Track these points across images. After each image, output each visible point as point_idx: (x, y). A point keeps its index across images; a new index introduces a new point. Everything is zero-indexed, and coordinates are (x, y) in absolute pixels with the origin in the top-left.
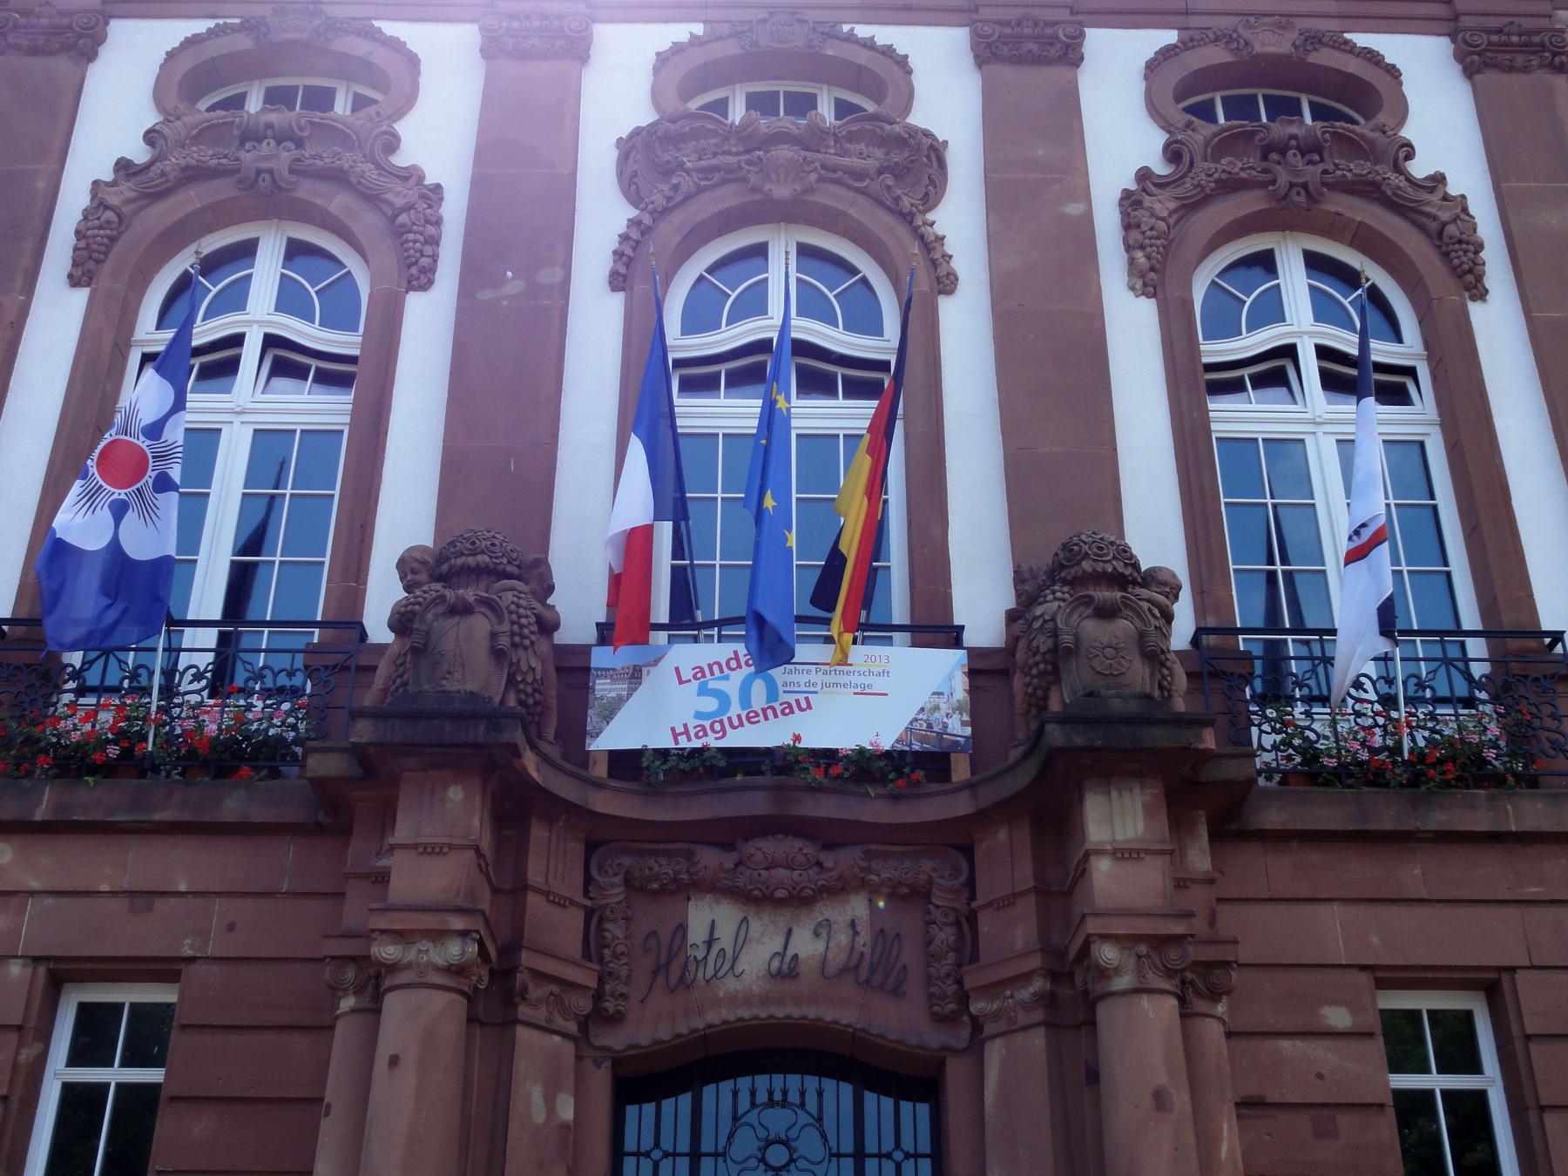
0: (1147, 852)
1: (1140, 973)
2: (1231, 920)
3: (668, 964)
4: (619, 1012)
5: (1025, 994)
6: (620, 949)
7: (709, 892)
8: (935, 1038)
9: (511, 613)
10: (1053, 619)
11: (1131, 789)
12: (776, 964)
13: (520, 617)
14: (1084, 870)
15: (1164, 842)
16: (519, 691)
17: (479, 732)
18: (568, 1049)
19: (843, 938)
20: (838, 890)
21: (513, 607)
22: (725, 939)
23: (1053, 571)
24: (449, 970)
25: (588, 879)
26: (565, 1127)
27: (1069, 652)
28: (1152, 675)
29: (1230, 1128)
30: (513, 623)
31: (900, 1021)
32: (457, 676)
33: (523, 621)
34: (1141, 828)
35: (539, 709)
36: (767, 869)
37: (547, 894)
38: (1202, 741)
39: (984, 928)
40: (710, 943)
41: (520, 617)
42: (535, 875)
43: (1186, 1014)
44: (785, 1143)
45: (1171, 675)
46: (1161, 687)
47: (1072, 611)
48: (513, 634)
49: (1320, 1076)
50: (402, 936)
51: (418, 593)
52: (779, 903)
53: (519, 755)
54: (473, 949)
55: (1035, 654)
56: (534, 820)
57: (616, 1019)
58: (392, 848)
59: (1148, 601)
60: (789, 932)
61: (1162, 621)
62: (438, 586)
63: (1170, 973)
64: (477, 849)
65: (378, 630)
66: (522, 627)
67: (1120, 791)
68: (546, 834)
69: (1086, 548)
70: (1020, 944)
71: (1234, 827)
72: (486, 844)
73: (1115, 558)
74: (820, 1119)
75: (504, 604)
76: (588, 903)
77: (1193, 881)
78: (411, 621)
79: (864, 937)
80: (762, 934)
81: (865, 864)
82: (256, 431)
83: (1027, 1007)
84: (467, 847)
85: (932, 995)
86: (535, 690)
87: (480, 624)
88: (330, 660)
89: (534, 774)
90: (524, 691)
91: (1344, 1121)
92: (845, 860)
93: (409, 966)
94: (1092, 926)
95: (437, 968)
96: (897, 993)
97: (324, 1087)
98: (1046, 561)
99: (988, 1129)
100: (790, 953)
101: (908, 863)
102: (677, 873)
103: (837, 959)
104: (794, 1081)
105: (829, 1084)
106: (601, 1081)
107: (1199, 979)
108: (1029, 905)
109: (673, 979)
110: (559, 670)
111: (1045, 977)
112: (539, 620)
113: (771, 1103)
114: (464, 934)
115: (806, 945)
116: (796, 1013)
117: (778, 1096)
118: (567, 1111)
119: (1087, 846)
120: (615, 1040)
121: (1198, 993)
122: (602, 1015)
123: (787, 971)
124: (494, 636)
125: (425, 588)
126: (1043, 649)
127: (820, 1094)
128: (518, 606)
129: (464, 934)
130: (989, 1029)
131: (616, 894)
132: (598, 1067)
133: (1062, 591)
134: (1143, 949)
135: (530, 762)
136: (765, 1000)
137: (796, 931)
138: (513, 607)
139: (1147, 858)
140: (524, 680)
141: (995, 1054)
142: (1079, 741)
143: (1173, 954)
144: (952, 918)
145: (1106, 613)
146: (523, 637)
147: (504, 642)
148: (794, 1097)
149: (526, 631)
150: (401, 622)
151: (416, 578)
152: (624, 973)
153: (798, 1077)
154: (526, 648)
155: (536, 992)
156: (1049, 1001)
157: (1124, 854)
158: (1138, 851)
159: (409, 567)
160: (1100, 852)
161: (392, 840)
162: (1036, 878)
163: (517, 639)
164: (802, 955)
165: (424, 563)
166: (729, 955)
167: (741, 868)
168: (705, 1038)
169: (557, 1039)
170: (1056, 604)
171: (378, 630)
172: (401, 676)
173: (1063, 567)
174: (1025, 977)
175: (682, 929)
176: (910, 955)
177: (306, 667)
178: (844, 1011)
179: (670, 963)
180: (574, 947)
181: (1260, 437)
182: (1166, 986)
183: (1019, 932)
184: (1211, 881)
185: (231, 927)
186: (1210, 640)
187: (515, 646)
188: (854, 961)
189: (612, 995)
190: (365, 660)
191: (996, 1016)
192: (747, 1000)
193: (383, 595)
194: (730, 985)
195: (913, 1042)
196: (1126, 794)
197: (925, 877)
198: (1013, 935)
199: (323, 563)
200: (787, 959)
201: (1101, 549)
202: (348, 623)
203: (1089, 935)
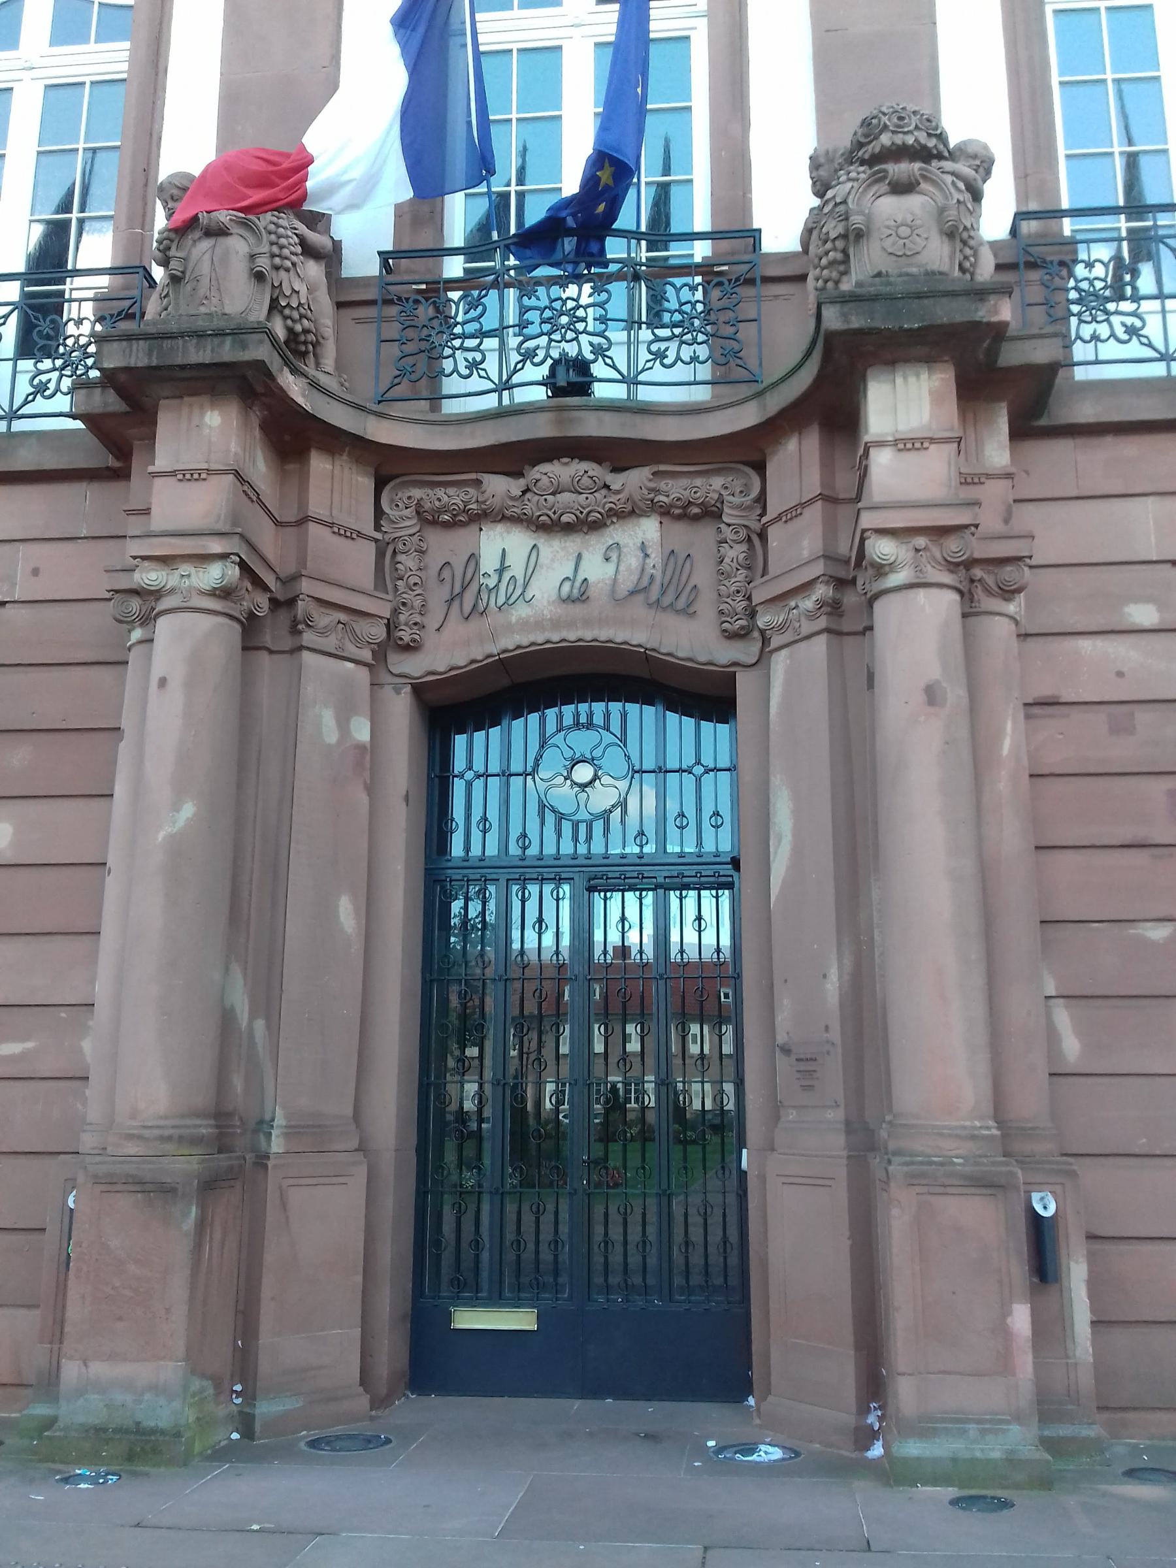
0: (932, 440)
1: (918, 568)
2: (1029, 517)
3: (461, 594)
4: (414, 641)
5: (808, 604)
6: (412, 580)
7: (500, 521)
8: (724, 653)
10: (844, 202)
11: (918, 376)
12: (566, 587)
14: (866, 467)
15: (952, 429)
16: (285, 318)
17: (227, 352)
18: (363, 675)
19: (632, 561)
20: (629, 513)
21: (272, 227)
22: (517, 568)
23: (852, 152)
24: (213, 593)
25: (379, 513)
26: (360, 748)
27: (859, 235)
28: (952, 257)
29: (1014, 722)
30: (272, 244)
31: (692, 640)
32: (214, 301)
33: (283, 241)
34: (926, 416)
36: (553, 494)
37: (331, 525)
38: (996, 312)
39: (773, 543)
40: (501, 571)
42: (317, 505)
43: (969, 612)
44: (591, 761)
45: (975, 255)
46: (962, 269)
47: (865, 190)
48: (273, 256)
49: (1120, 674)
50: (165, 560)
52: (568, 529)
54: (233, 572)
55: (826, 242)
57: (410, 648)
59: (953, 174)
60: (579, 557)
61: (967, 197)
63: (953, 567)
66: (282, 247)
67: (905, 378)
68: (329, 467)
69: (885, 119)
70: (806, 554)
71: (1043, 422)
73: (917, 127)
74: (624, 740)
76: (378, 536)
77: (989, 476)
79: (655, 558)
80: (553, 560)
81: (652, 485)
82: (46, 87)
83: (811, 616)
84: (225, 472)
85: (721, 612)
86: (302, 316)
89: (300, 400)
91: (1143, 717)
92: (635, 480)
93: (172, 591)
94: (868, 520)
95: (202, 593)
96: (688, 612)
97: (120, 717)
98: (844, 141)
99: (772, 737)
100: (580, 578)
101: (698, 482)
102: (466, 503)
103: (627, 582)
104: (599, 707)
105: (633, 708)
106: (401, 709)
107: (982, 577)
108: (815, 513)
109: (467, 608)
111: (827, 583)
113: (577, 725)
114: (224, 557)
115: (596, 570)
116: (588, 635)
117: (583, 719)
118: (362, 731)
119: (867, 438)
120: (415, 666)
121: (989, 592)
122: (395, 642)
123: (579, 596)
124: (252, 257)
126: (833, 235)
127: (624, 716)
128: (278, 226)
129: (224, 557)
130: (776, 641)
131: (410, 525)
132: (398, 691)
133: (861, 172)
134: (921, 541)
136: (556, 624)
137: (586, 555)
138: (272, 227)
139: (933, 447)
141: (780, 663)
142: (856, 323)
143: (953, 545)
144: (743, 533)
145: (902, 188)
147: (264, 263)
148: (598, 719)
149: (286, 252)
152: (417, 603)
153: (619, 705)
154: (287, 270)
155: (325, 618)
156: (834, 608)
157: (906, 444)
158: (922, 440)
160: (881, 444)
162: (823, 485)
163: (277, 260)
164: (591, 579)
165: (185, 189)
166: (520, 582)
167: (529, 495)
168: (503, 664)
169: (350, 665)
170: (850, 185)
173: (861, 145)
174: (807, 587)
175: (474, 558)
176: (703, 576)
178: (637, 632)
179: (466, 592)
180: (366, 579)
181: (1102, 5)
182: (947, 578)
183: (806, 543)
184: (1009, 476)
185: (36, 572)
186: (1029, 227)
187: (277, 268)
188: (645, 582)
189: (406, 624)
191: (782, 628)
192: (539, 625)
194: (521, 612)
195: (702, 659)
196: (912, 380)
197: (716, 496)
198: (798, 547)
200: (577, 584)
201: (901, 118)
203: (864, 531)
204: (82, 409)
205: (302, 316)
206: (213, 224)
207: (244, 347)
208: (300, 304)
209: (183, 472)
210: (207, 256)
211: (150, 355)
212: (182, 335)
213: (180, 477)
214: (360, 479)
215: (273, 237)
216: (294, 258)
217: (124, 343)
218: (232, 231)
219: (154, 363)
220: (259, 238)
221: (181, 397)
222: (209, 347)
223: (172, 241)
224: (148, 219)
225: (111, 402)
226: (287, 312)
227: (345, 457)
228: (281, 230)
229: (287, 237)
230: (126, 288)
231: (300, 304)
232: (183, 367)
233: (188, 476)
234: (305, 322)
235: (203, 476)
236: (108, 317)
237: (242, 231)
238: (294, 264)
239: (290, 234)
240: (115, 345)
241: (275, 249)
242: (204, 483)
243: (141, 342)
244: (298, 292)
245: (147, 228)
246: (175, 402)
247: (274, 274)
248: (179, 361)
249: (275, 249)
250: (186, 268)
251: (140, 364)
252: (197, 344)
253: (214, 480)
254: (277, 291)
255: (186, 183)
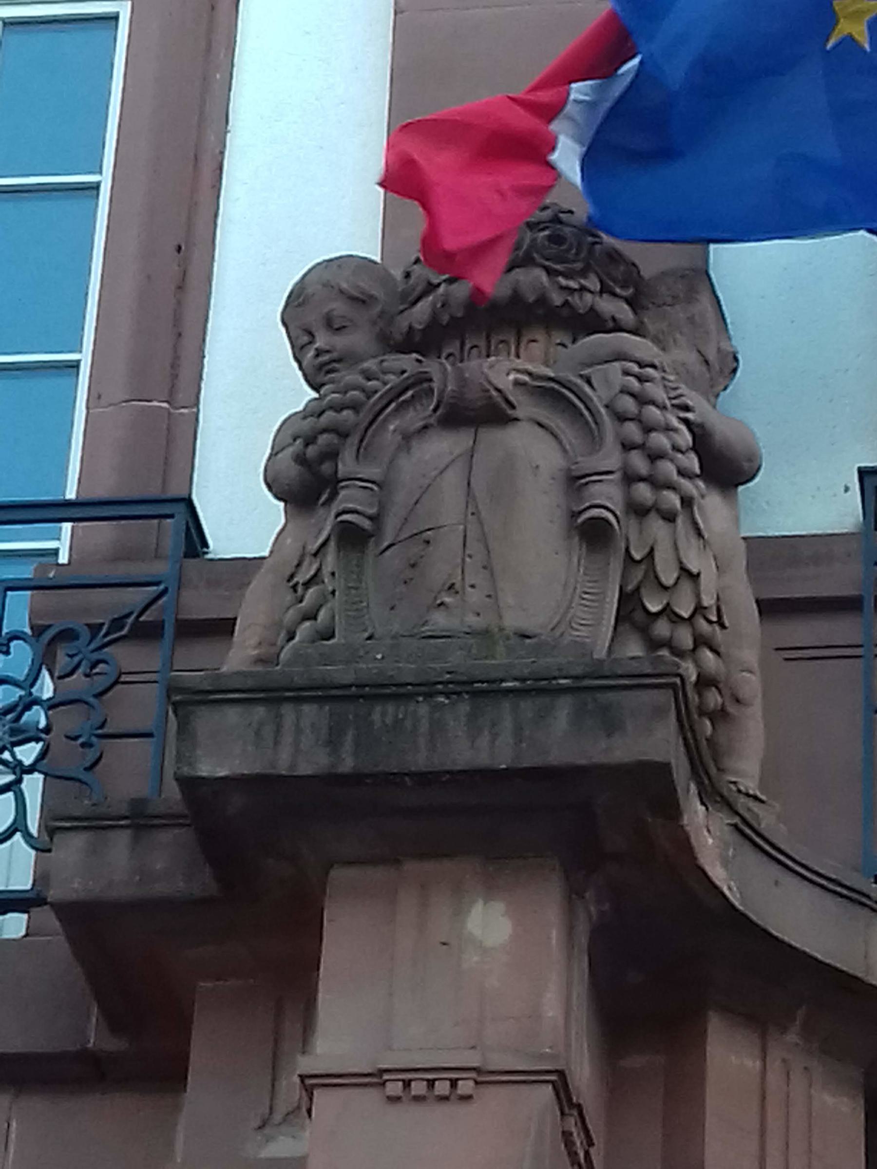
9: (622, 418)
13: (648, 429)
17: (560, 739)
21: (628, 404)
30: (627, 447)
32: (474, 597)
33: (659, 440)
35: (713, 699)
41: (648, 429)
48: (630, 478)
51: (351, 377)
53: (671, 809)
56: (711, 1013)
58: (310, 1084)
62: (408, 362)
64: (561, 1085)
65: (240, 512)
66: (655, 456)
68: (753, 1064)
72: (584, 1075)
75: (598, 398)
78: (332, 455)
87: (533, 450)
88: (106, 604)
89: (718, 874)
90: (668, 644)
110: (769, 609)
112: (702, 440)
124: (575, 482)
125: (370, 364)
128: (643, 400)
135: (708, 835)
138: (628, 404)
140: (668, 611)
146: (658, 484)
147: (607, 496)
149: (668, 469)
150: (305, 475)
151: (341, 342)
154: (670, 517)
159: (320, 313)
161: (306, 1064)
163: (643, 492)
165: (362, 301)
171: (240, 512)
172: (311, 616)
177: (38, 631)
187: (639, 511)
190: (200, 605)
193: (250, 391)
199: (96, 187)
202: (153, 505)
204: (70, 886)
205: (701, 641)
206: (473, 394)
207: (611, 724)
208: (699, 609)
209: (407, 1075)
210: (453, 480)
211: (333, 742)
212: (428, 689)
213: (394, 1089)
214: (829, 1099)
215: (632, 430)
216: (686, 485)
217: (260, 712)
218: (519, 413)
219: (347, 764)
220: (593, 438)
221: (396, 862)
222: (507, 723)
223: (344, 435)
224: (185, 373)
225: (164, 867)
226: (662, 629)
227: (792, 1037)
228: (653, 412)
229: (668, 429)
230: (124, 554)
231: (699, 609)
232: (426, 779)
233: (419, 1088)
234: (708, 655)
235: (466, 1087)
236: (85, 634)
237: (543, 414)
238: (687, 502)
239: (675, 423)
240: (232, 715)
241: (639, 463)
242: (463, 1109)
243: (306, 708)
244: (695, 577)
245: (181, 398)
246: (378, 874)
247: (632, 527)
248: (420, 759)
249: (639, 463)
250: (382, 506)
251: (305, 769)
252: (472, 717)
253: (495, 1099)
254: (638, 574)
255: (367, 285)
